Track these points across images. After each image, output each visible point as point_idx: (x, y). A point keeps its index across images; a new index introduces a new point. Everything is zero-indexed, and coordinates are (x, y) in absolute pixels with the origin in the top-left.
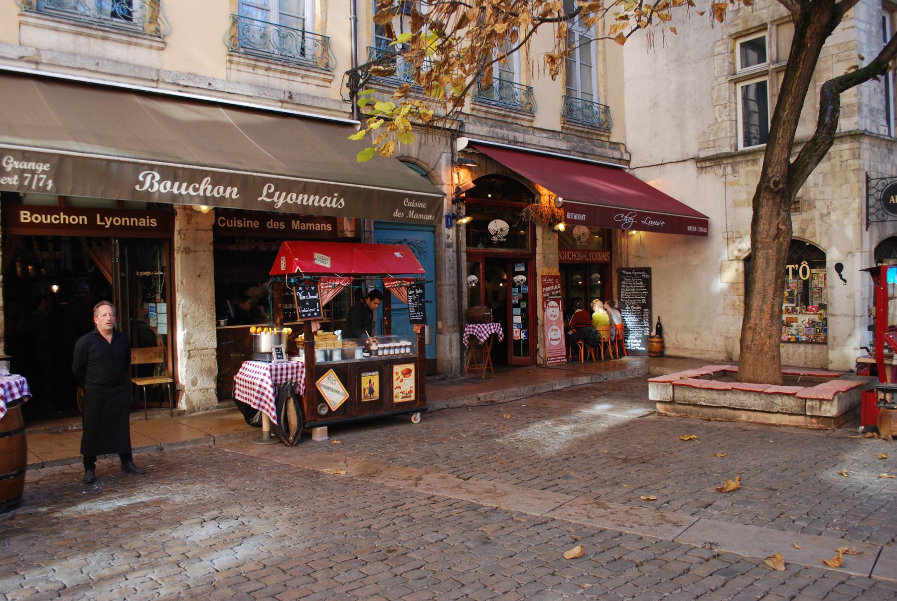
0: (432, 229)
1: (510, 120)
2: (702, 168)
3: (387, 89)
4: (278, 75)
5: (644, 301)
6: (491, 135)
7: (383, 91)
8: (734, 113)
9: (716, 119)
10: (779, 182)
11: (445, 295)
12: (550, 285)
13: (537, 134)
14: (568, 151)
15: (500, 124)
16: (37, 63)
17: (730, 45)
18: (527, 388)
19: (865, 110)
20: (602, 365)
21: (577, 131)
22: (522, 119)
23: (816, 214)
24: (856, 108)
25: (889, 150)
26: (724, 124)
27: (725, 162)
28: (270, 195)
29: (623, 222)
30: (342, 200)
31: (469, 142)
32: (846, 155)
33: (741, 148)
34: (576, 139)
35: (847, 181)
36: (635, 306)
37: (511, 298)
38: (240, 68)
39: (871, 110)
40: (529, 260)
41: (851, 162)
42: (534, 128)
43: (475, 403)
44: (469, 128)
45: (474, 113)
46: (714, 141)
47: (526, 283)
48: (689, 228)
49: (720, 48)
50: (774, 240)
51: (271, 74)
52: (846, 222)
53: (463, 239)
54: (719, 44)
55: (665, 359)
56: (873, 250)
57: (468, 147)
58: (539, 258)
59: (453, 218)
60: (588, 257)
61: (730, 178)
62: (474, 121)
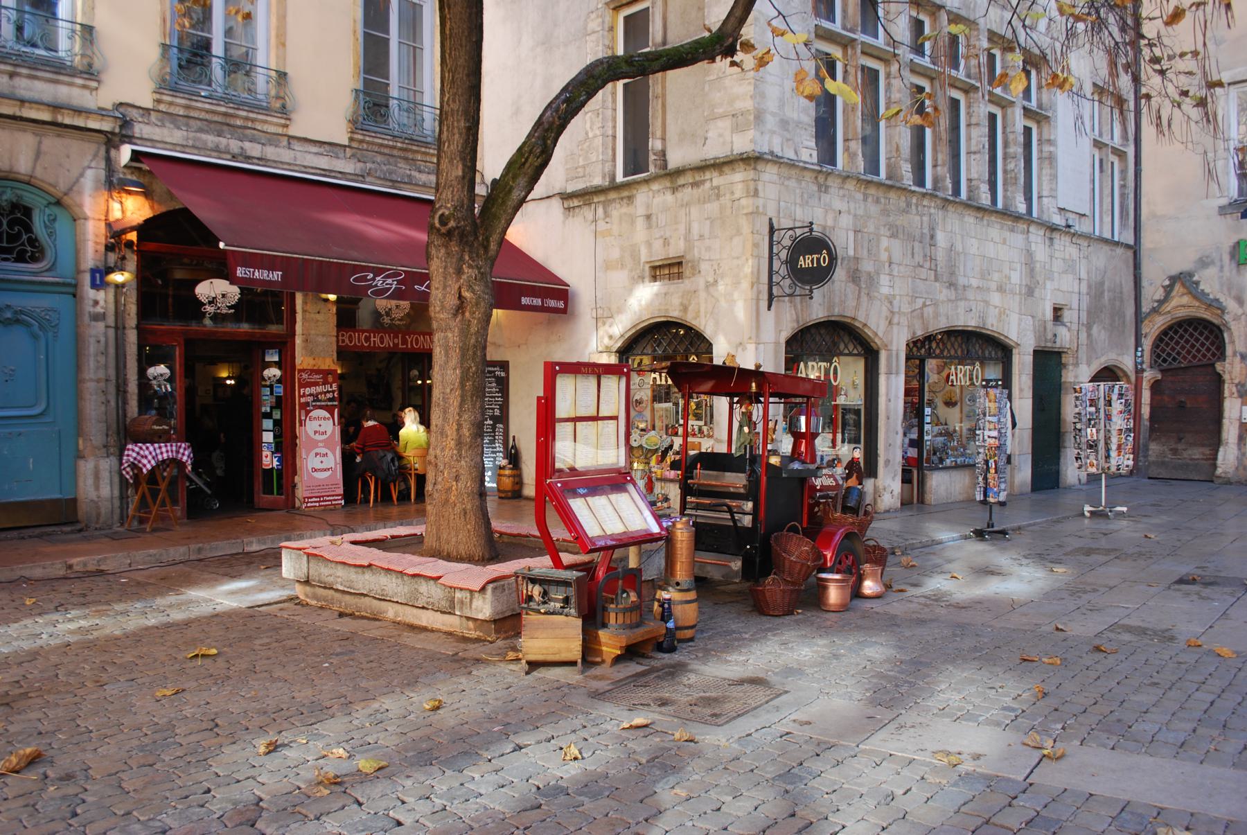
0: (71, 290)
1: (239, 122)
2: (569, 209)
5: (497, 413)
6: (191, 143)
8: (610, 124)
9: (587, 134)
10: (448, 218)
11: (88, 396)
12: (316, 384)
13: (297, 146)
14: (361, 177)
15: (218, 127)
17: (608, 19)
18: (182, 549)
19: (771, 122)
20: (413, 507)
21: (381, 145)
22: (265, 122)
23: (700, 282)
24: (752, 118)
25: (820, 186)
26: (596, 140)
27: (596, 200)
29: (370, 286)
31: (133, 151)
32: (739, 190)
33: (620, 178)
34: (379, 158)
35: (739, 233)
37: (260, 403)
39: (784, 123)
40: (285, 345)
41: (744, 202)
42: (290, 137)
43: (62, 573)
44: (139, 129)
45: (162, 107)
46: (584, 167)
47: (279, 381)
48: (525, 301)
49: (594, 25)
50: (455, 315)
52: (736, 295)
53: (133, 309)
54: (593, 16)
55: (523, 503)
56: (783, 341)
57: (132, 160)
58: (298, 341)
59: (99, 276)
60: (404, 342)
61: (602, 225)
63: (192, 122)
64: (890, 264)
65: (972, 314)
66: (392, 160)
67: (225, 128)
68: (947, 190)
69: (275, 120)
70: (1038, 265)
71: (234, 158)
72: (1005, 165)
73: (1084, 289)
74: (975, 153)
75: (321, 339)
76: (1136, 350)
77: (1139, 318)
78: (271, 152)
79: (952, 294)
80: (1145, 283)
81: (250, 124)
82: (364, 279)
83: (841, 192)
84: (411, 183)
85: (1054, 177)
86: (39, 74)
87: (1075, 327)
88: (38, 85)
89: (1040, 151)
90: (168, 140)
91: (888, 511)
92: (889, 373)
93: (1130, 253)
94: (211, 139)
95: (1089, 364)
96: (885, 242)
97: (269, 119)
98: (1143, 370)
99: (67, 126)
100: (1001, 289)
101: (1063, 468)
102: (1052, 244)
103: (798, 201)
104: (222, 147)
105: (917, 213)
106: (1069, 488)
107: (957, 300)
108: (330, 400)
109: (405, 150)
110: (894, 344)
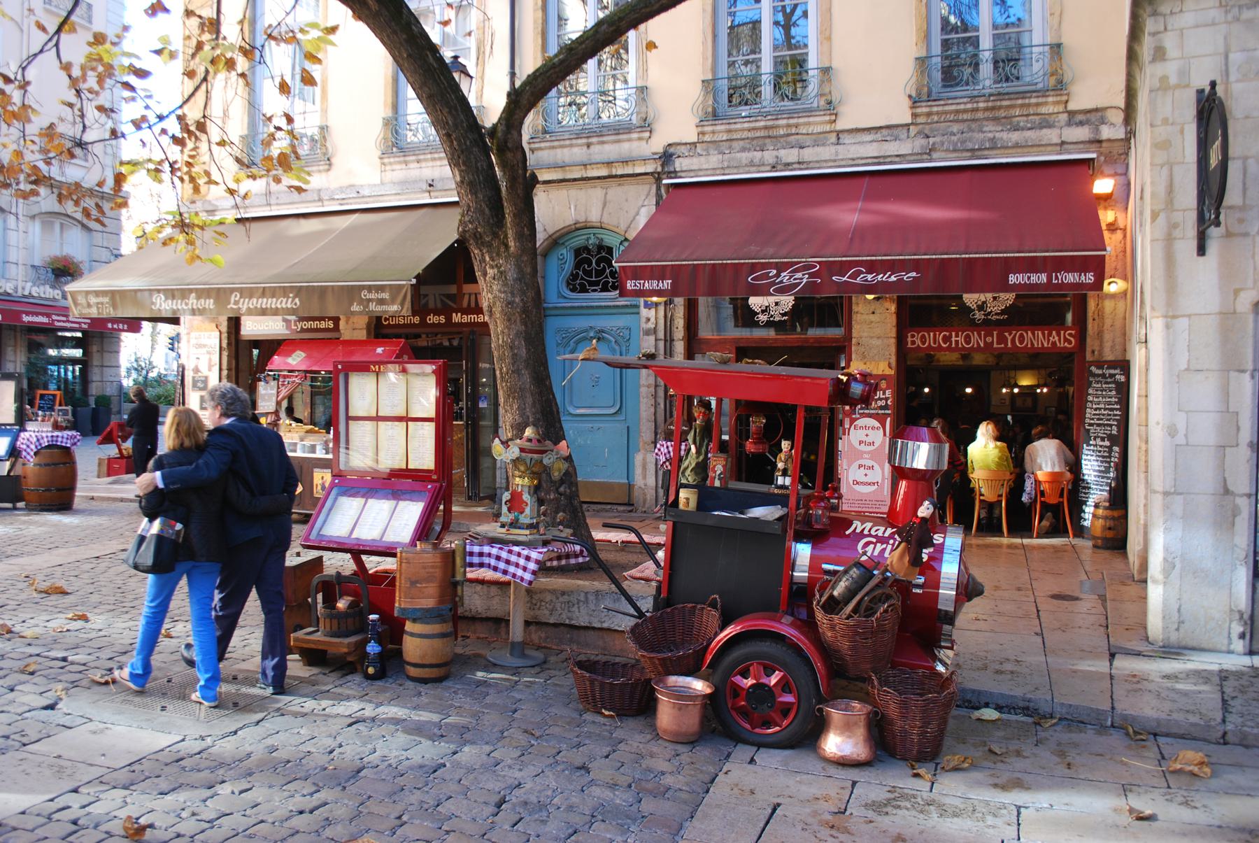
3: (556, 143)
4: (430, 164)
6: (726, 164)
7: (553, 147)
13: (846, 139)
14: (917, 156)
15: (761, 142)
16: (320, 200)
21: (957, 112)
22: (809, 124)
28: (236, 303)
29: (774, 283)
30: (297, 300)
36: (1103, 439)
38: (395, 167)
45: (707, 138)
51: (423, 164)
60: (1002, 339)
62: (707, 150)
63: (735, 144)
66: (973, 126)
67: (768, 141)
71: (774, 168)
75: (875, 342)
78: (808, 154)
81: (794, 131)
82: (766, 276)
84: (994, 146)
86: (605, 139)
88: (607, 147)
90: (705, 167)
94: (745, 157)
97: (811, 119)
99: (622, 176)
102: (324, 129)
104: (756, 161)
108: (881, 408)
109: (993, 108)
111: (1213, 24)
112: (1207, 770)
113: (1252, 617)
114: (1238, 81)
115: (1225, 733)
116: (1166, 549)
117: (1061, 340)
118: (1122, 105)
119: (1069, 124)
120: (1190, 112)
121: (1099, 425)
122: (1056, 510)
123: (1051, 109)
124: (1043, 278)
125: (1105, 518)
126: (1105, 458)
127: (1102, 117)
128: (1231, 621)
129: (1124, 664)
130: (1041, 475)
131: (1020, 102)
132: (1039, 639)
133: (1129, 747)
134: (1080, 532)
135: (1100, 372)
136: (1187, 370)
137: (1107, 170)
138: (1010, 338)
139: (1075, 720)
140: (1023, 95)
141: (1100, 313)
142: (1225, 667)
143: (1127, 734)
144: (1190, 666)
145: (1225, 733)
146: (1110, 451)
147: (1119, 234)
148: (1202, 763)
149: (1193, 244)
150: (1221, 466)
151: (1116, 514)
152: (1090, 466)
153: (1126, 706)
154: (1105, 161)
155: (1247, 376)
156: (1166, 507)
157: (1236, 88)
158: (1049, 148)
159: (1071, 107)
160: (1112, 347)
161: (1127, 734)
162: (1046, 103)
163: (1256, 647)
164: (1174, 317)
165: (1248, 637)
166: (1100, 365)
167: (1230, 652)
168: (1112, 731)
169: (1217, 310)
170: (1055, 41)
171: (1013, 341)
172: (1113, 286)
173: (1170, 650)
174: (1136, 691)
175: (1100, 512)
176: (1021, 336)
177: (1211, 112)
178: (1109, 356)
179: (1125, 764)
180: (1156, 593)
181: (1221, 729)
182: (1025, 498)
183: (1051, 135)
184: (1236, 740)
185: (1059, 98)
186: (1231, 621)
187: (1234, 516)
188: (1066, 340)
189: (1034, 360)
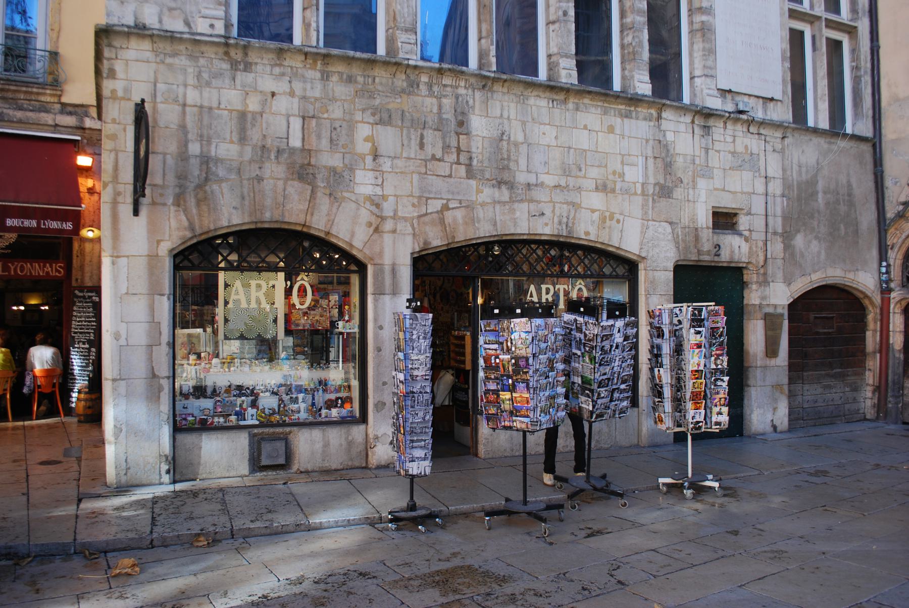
25: (234, 65)
36: (84, 343)
64: (376, 157)
65: (544, 219)
68: (490, 65)
69: (48, 92)
70: (680, 160)
72: (622, 39)
73: (776, 188)
74: (553, 22)
76: (880, 266)
77: (882, 225)
79: (505, 195)
80: (888, 183)
83: (277, 70)
85: (710, 52)
87: (759, 236)
89: (691, 23)
91: (379, 467)
92: (379, 292)
93: (866, 148)
95: (788, 281)
96: (363, 131)
98: (890, 290)
100: (603, 188)
101: (747, 410)
103: (191, 80)
105: (431, 94)
106: (754, 437)
107: (512, 201)
110: (395, 255)
111: (148, 62)
112: (137, 569)
113: (174, 458)
114: (162, 102)
115: (152, 540)
116: (116, 419)
117: (54, 270)
118: (95, 104)
119: (62, 112)
120: (130, 118)
121: (81, 333)
122: (50, 397)
123: (49, 99)
124: (34, 223)
125: (86, 400)
126: (86, 357)
127: (86, 112)
128: (160, 463)
129: (88, 505)
130: (38, 373)
131: (24, 89)
132: (25, 498)
133: (85, 566)
134: (69, 412)
135: (81, 294)
136: (127, 293)
137: (89, 150)
138: (12, 268)
139: (47, 554)
140: (27, 84)
141: (82, 252)
142: (156, 495)
143: (85, 556)
144: (134, 498)
145: (152, 540)
146: (89, 350)
147: (96, 197)
148: (134, 565)
149: (130, 208)
150: (150, 359)
151: (93, 396)
152: (77, 362)
153: (84, 536)
154: (88, 144)
155: (165, 298)
156: (114, 389)
157: (161, 107)
158: (46, 128)
159: (64, 100)
160: (91, 277)
161: (85, 556)
162: (44, 94)
163: (178, 477)
164: (118, 257)
165: (172, 472)
166: (81, 289)
167: (161, 484)
168: (75, 557)
169: (146, 253)
170: (53, 50)
171: (15, 270)
172: (88, 233)
173: (122, 489)
174: (93, 523)
175: (82, 396)
176: (22, 267)
177: (141, 117)
178: (89, 284)
179: (79, 579)
180: (110, 451)
181: (149, 538)
182: (25, 390)
183: (48, 118)
184: (160, 543)
185: (55, 92)
186: (160, 463)
187: (160, 392)
188: (57, 271)
189: (36, 285)
